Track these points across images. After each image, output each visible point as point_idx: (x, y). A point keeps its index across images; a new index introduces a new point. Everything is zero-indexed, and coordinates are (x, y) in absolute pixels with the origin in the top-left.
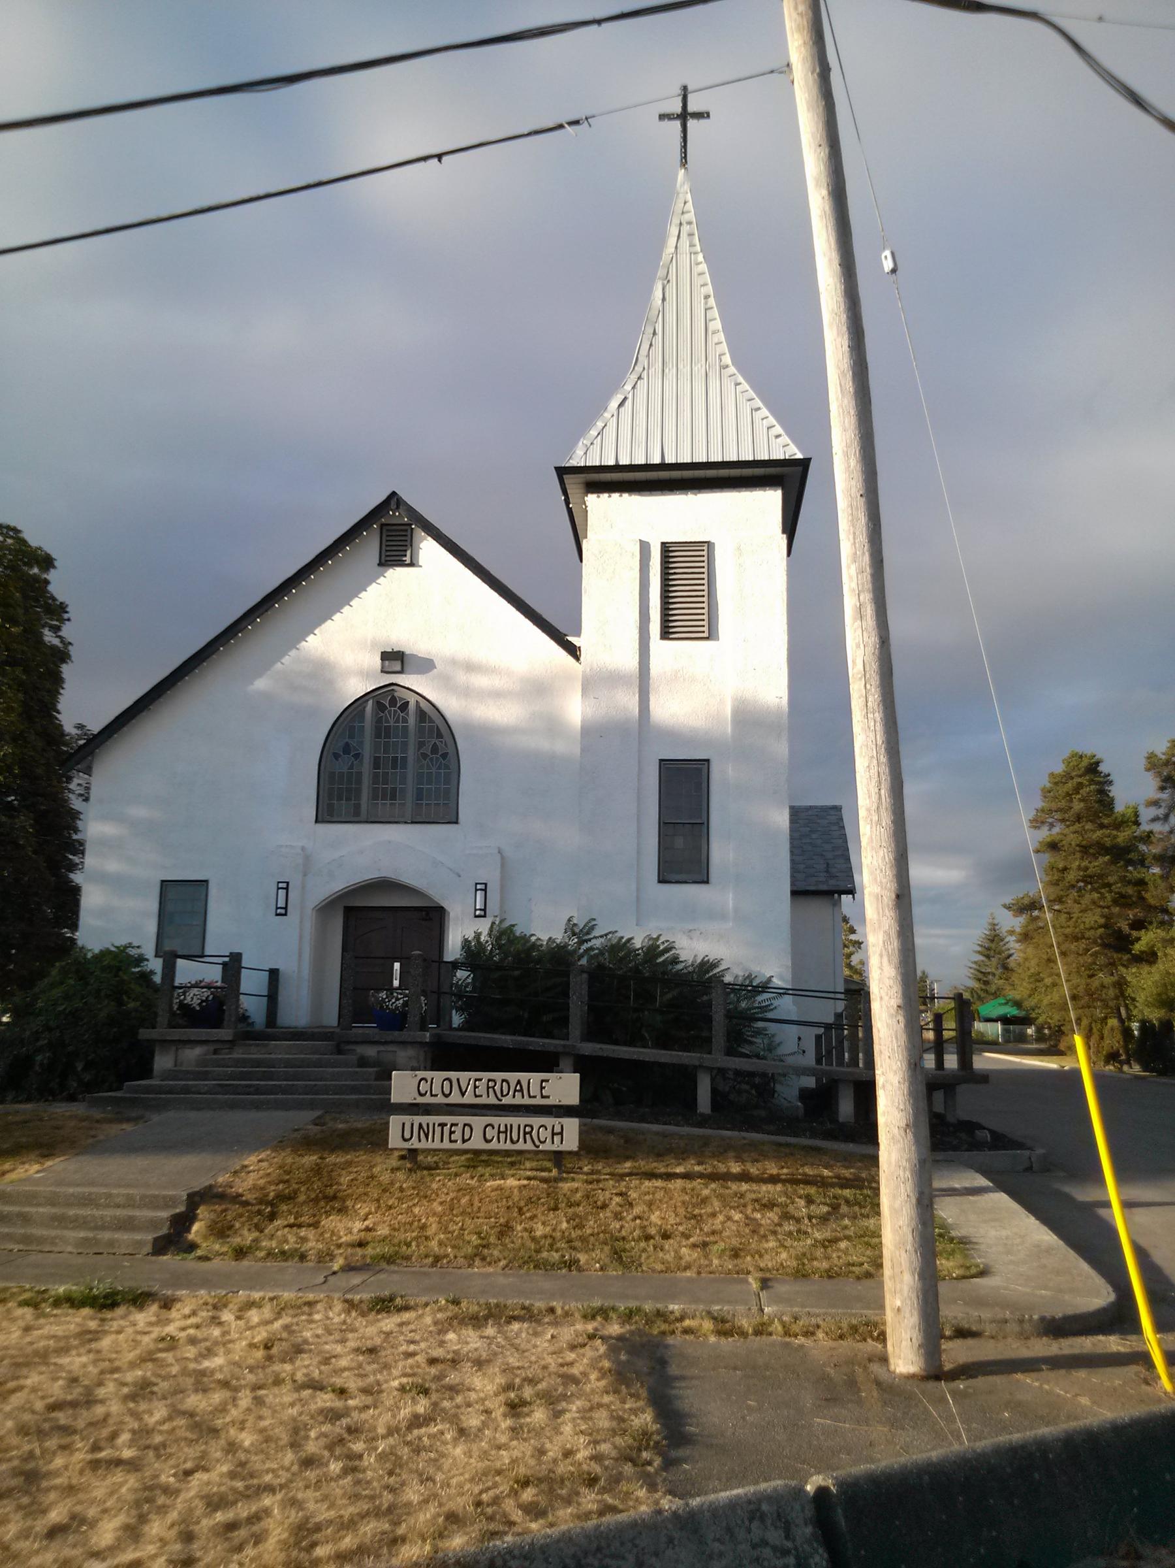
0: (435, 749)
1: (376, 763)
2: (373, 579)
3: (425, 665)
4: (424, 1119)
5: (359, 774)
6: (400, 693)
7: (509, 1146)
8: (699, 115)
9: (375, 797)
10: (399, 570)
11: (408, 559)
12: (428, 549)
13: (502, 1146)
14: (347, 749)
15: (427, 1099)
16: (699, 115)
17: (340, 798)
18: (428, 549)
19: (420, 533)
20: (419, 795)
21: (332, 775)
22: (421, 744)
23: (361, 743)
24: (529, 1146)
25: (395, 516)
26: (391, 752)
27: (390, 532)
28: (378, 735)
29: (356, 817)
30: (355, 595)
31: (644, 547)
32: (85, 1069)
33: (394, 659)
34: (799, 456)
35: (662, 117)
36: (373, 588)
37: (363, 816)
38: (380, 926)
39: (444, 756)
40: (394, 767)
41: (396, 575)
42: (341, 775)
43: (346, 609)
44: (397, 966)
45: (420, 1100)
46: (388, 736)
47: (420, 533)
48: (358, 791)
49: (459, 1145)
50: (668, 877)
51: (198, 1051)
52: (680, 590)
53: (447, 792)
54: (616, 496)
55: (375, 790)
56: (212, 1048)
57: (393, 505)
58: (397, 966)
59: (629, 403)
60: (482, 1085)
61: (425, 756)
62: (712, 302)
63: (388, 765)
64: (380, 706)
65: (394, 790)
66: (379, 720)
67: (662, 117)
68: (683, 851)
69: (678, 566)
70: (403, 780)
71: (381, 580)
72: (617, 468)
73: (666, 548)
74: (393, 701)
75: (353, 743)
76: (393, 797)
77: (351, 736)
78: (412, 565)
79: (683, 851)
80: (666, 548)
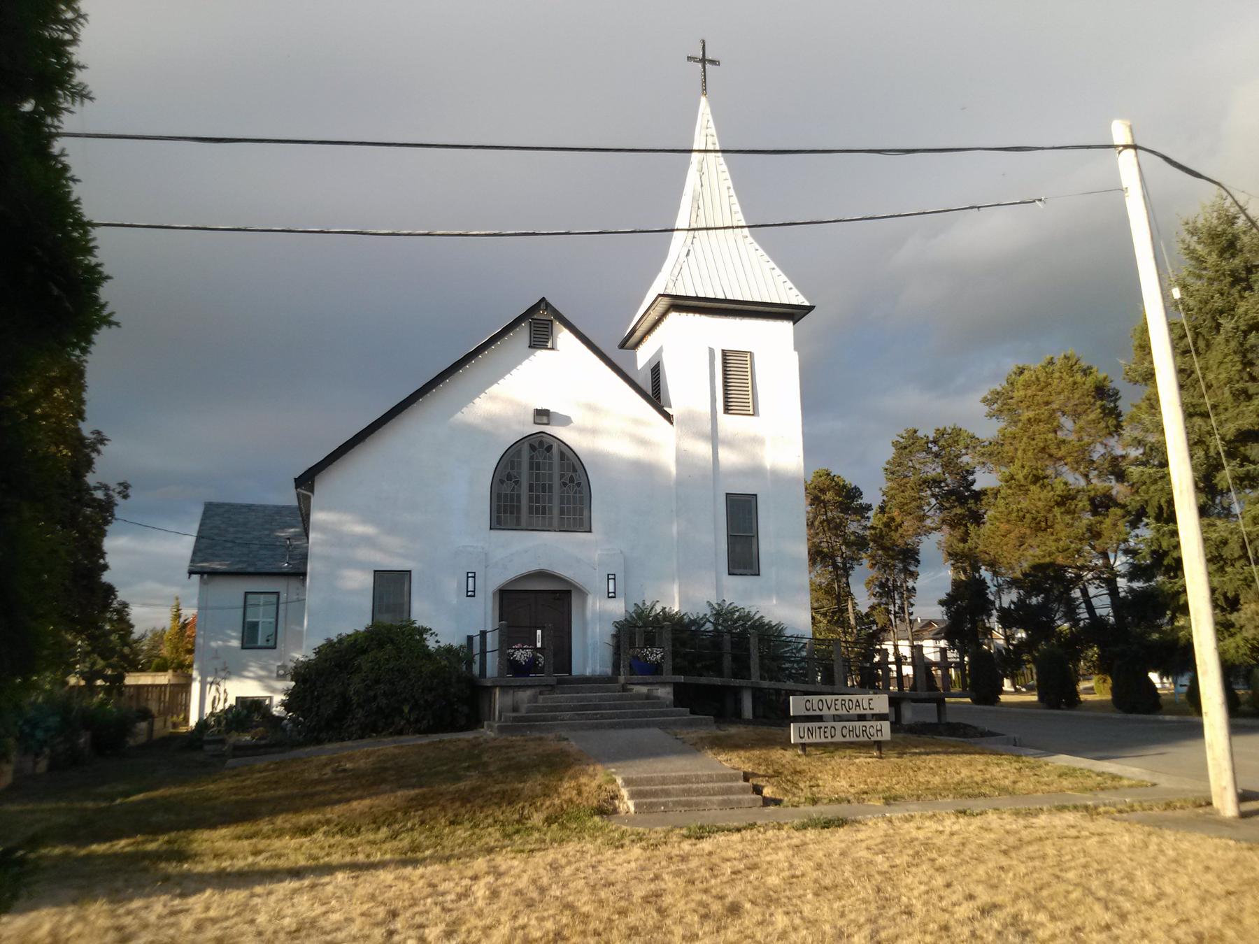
0: (572, 480)
1: (531, 488)
2: (527, 357)
3: (565, 421)
4: (810, 725)
5: (519, 496)
6: (547, 439)
7: (855, 739)
8: (713, 62)
9: (531, 512)
10: (544, 352)
11: (549, 345)
12: (564, 337)
13: (852, 739)
14: (509, 477)
15: (811, 713)
16: (713, 62)
17: (505, 512)
18: (564, 337)
19: (557, 325)
20: (562, 512)
21: (499, 496)
22: (562, 476)
23: (519, 474)
24: (866, 739)
25: (542, 314)
26: (541, 478)
27: (538, 324)
28: (531, 468)
29: (517, 526)
30: (514, 367)
31: (711, 351)
32: (411, 710)
33: (542, 415)
34: (807, 304)
35: (689, 58)
36: (526, 363)
37: (524, 524)
38: (537, 607)
39: (579, 484)
40: (544, 491)
41: (541, 354)
42: (506, 495)
43: (508, 376)
44: (539, 632)
45: (808, 713)
46: (538, 469)
47: (557, 325)
48: (519, 509)
49: (829, 740)
50: (736, 571)
51: (529, 693)
52: (733, 382)
53: (499, 511)
54: (691, 315)
55: (531, 508)
56: (538, 690)
57: (543, 306)
58: (539, 632)
59: (691, 253)
60: (839, 703)
61: (565, 484)
62: (732, 192)
63: (540, 489)
64: (532, 448)
65: (544, 508)
66: (532, 457)
67: (689, 58)
68: (743, 556)
69: (732, 365)
70: (550, 501)
71: (532, 357)
72: (697, 298)
73: (725, 353)
74: (541, 443)
75: (514, 473)
76: (544, 513)
77: (512, 468)
78: (552, 349)
79: (743, 556)
80: (725, 353)
